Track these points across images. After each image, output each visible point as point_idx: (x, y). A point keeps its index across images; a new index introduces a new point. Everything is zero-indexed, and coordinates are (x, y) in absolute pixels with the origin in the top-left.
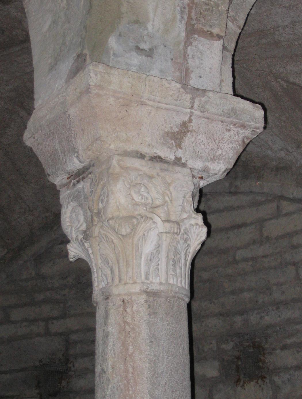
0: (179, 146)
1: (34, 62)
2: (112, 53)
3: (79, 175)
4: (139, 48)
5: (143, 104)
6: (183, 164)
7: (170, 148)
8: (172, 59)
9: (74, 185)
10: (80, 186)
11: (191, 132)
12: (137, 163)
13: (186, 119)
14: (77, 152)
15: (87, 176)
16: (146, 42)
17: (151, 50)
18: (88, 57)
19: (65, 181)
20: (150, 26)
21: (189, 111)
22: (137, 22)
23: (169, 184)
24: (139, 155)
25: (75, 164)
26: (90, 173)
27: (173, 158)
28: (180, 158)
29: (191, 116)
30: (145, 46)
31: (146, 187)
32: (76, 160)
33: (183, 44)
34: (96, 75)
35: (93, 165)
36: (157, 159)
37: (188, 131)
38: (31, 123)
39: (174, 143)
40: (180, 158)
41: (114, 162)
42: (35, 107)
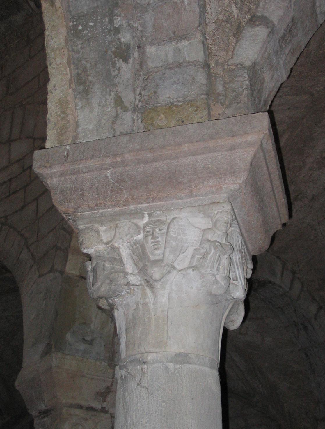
0: (104, 400)
1: (24, 337)
2: (68, 343)
3: (45, 413)
4: (85, 339)
5: (83, 376)
6: (106, 411)
7: (99, 402)
8: (105, 345)
9: (42, 418)
10: (46, 419)
11: (112, 391)
12: (78, 412)
13: (110, 384)
14: (44, 401)
15: (49, 415)
16: (89, 336)
17: (92, 340)
18: (53, 346)
19: (37, 414)
20: (92, 326)
21: (111, 380)
22: (85, 323)
23: (97, 424)
24: (79, 407)
25: (43, 407)
26: (51, 414)
27: (100, 407)
28: (105, 408)
29: (112, 383)
30: (88, 338)
31: (82, 426)
32: (43, 405)
33: (112, 336)
34: (56, 359)
35: (53, 410)
36: (90, 409)
37: (110, 391)
38: (20, 376)
39: (101, 399)
40: (105, 408)
41: (64, 411)
42: (23, 367)
